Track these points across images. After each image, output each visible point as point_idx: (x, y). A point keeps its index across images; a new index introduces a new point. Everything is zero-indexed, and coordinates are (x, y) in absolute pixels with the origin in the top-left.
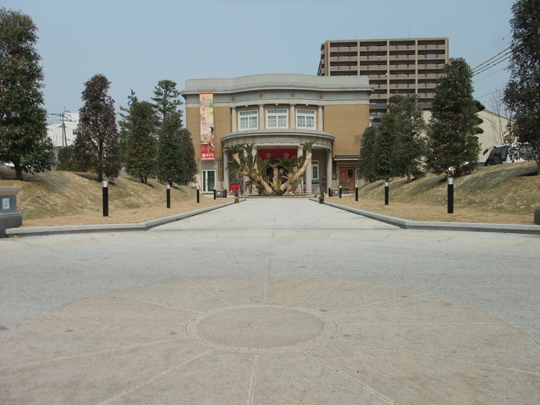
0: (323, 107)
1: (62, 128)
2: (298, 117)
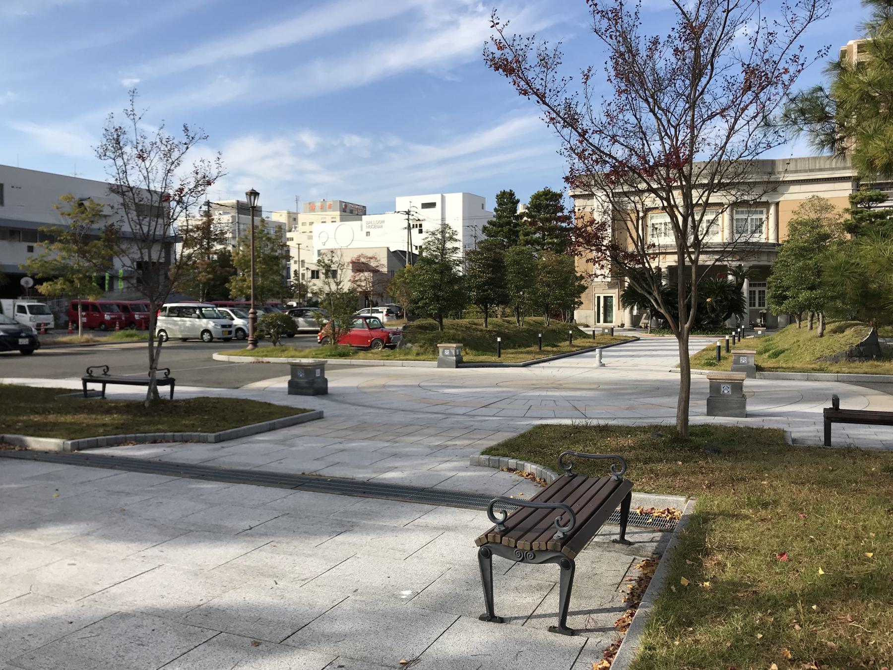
0: (777, 204)
1: (407, 230)
2: (737, 220)
